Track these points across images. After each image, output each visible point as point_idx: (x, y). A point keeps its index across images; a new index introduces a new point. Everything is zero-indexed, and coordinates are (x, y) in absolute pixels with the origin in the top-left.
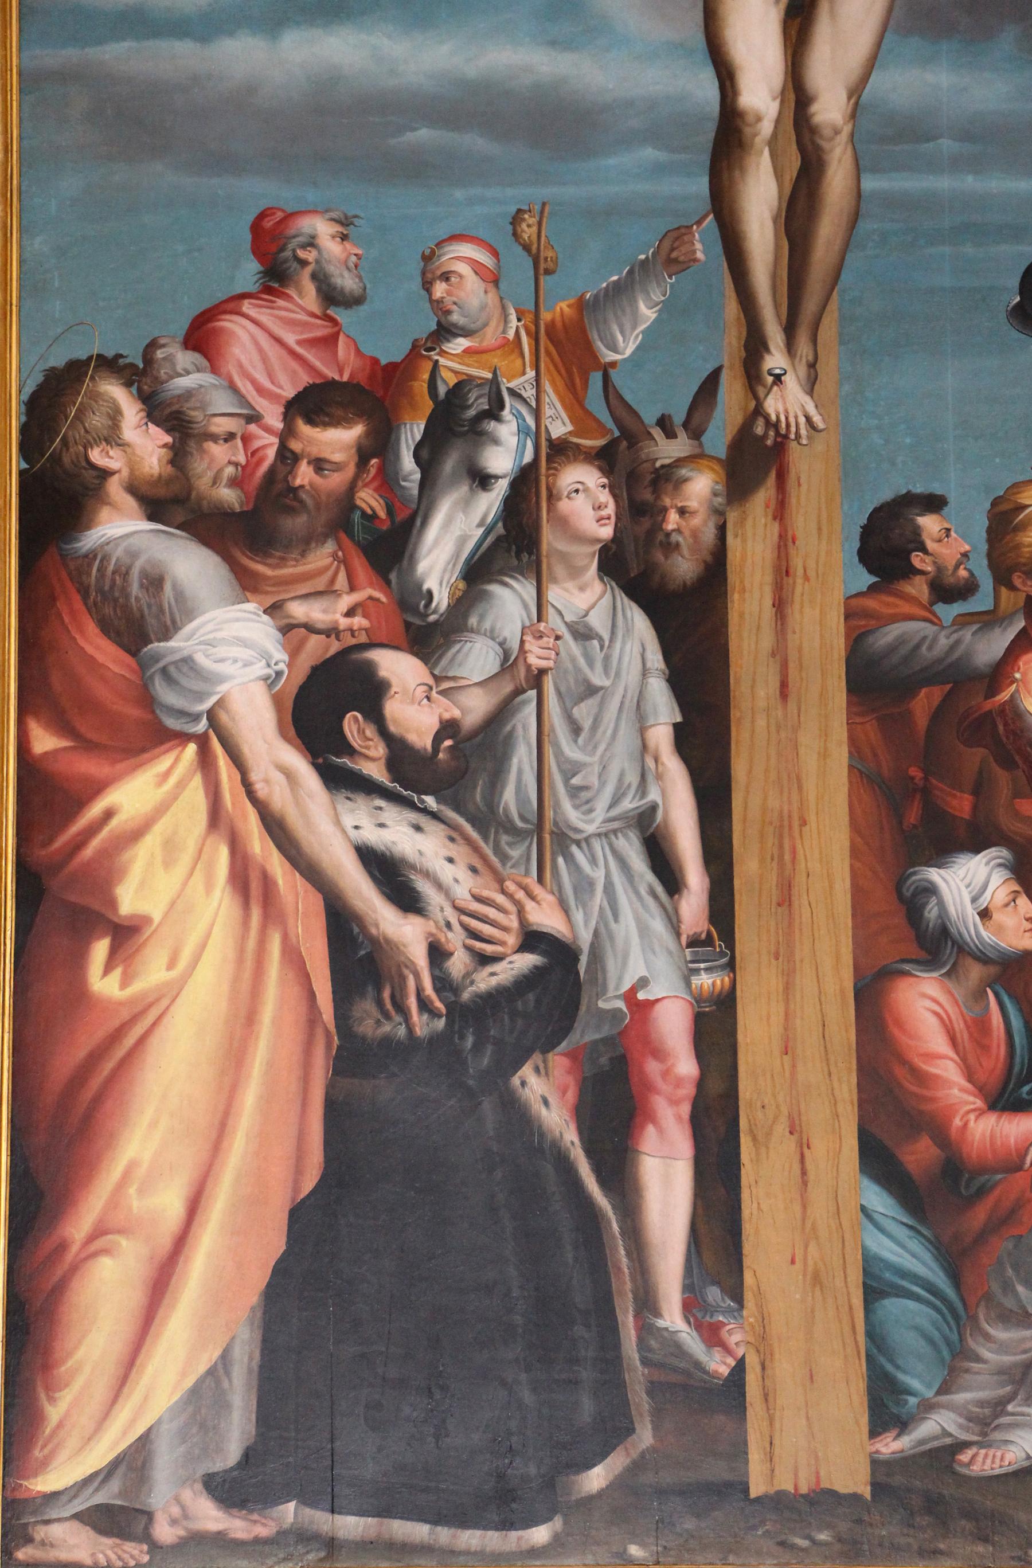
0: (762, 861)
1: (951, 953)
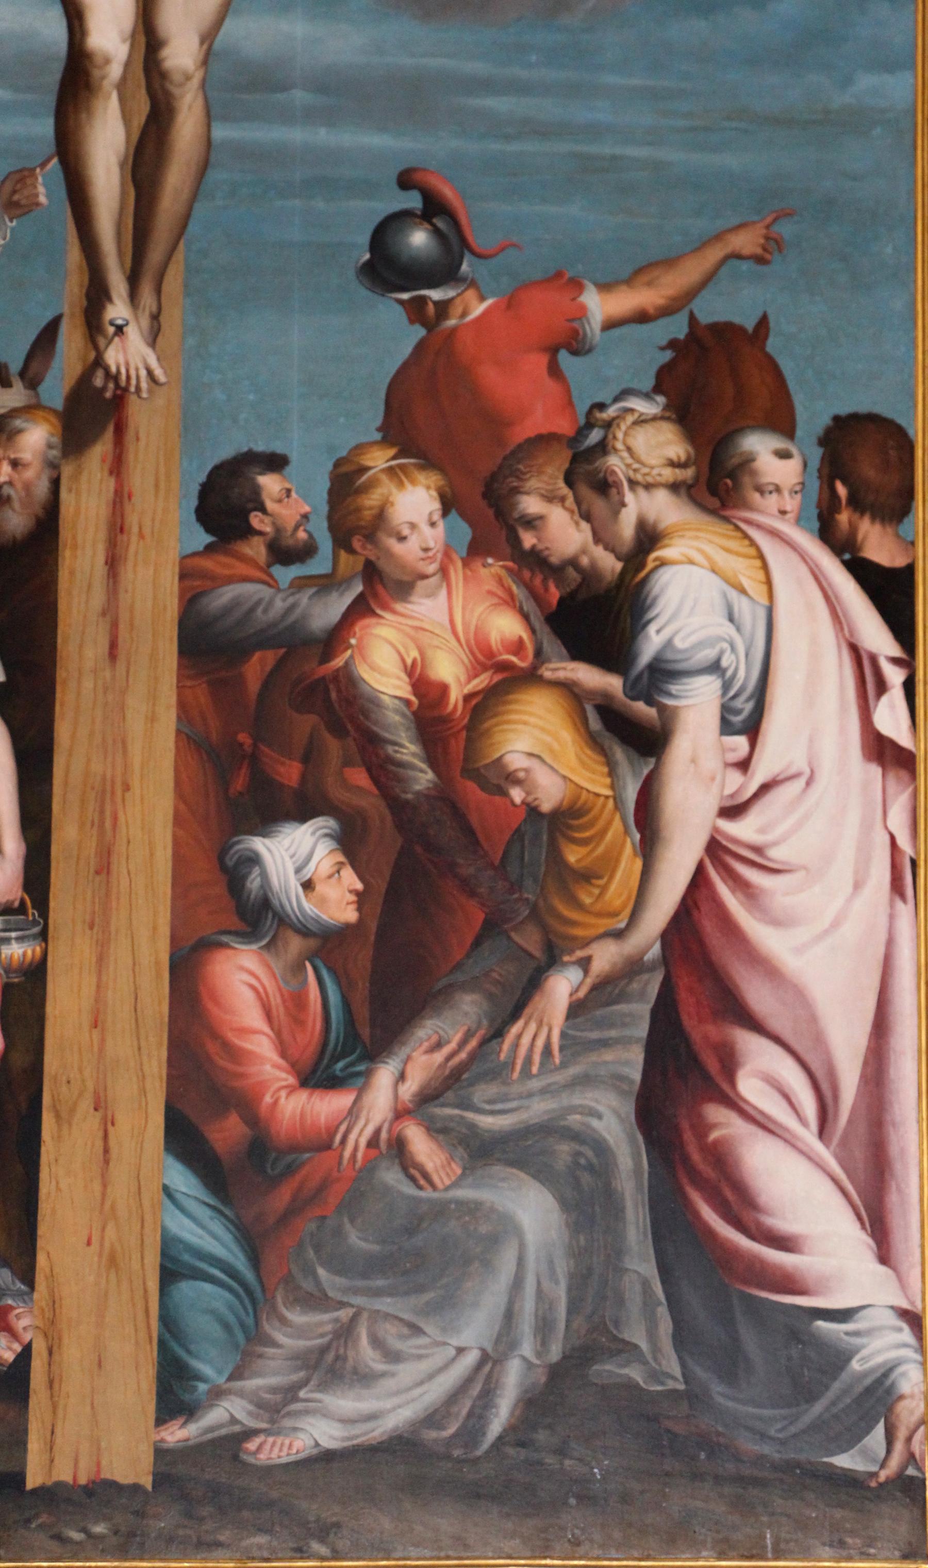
0: (82, 825)
1: (271, 926)
